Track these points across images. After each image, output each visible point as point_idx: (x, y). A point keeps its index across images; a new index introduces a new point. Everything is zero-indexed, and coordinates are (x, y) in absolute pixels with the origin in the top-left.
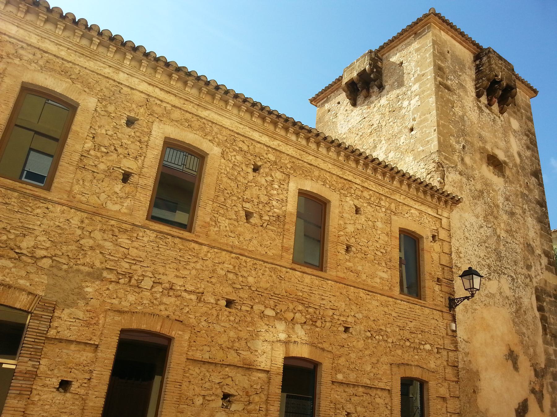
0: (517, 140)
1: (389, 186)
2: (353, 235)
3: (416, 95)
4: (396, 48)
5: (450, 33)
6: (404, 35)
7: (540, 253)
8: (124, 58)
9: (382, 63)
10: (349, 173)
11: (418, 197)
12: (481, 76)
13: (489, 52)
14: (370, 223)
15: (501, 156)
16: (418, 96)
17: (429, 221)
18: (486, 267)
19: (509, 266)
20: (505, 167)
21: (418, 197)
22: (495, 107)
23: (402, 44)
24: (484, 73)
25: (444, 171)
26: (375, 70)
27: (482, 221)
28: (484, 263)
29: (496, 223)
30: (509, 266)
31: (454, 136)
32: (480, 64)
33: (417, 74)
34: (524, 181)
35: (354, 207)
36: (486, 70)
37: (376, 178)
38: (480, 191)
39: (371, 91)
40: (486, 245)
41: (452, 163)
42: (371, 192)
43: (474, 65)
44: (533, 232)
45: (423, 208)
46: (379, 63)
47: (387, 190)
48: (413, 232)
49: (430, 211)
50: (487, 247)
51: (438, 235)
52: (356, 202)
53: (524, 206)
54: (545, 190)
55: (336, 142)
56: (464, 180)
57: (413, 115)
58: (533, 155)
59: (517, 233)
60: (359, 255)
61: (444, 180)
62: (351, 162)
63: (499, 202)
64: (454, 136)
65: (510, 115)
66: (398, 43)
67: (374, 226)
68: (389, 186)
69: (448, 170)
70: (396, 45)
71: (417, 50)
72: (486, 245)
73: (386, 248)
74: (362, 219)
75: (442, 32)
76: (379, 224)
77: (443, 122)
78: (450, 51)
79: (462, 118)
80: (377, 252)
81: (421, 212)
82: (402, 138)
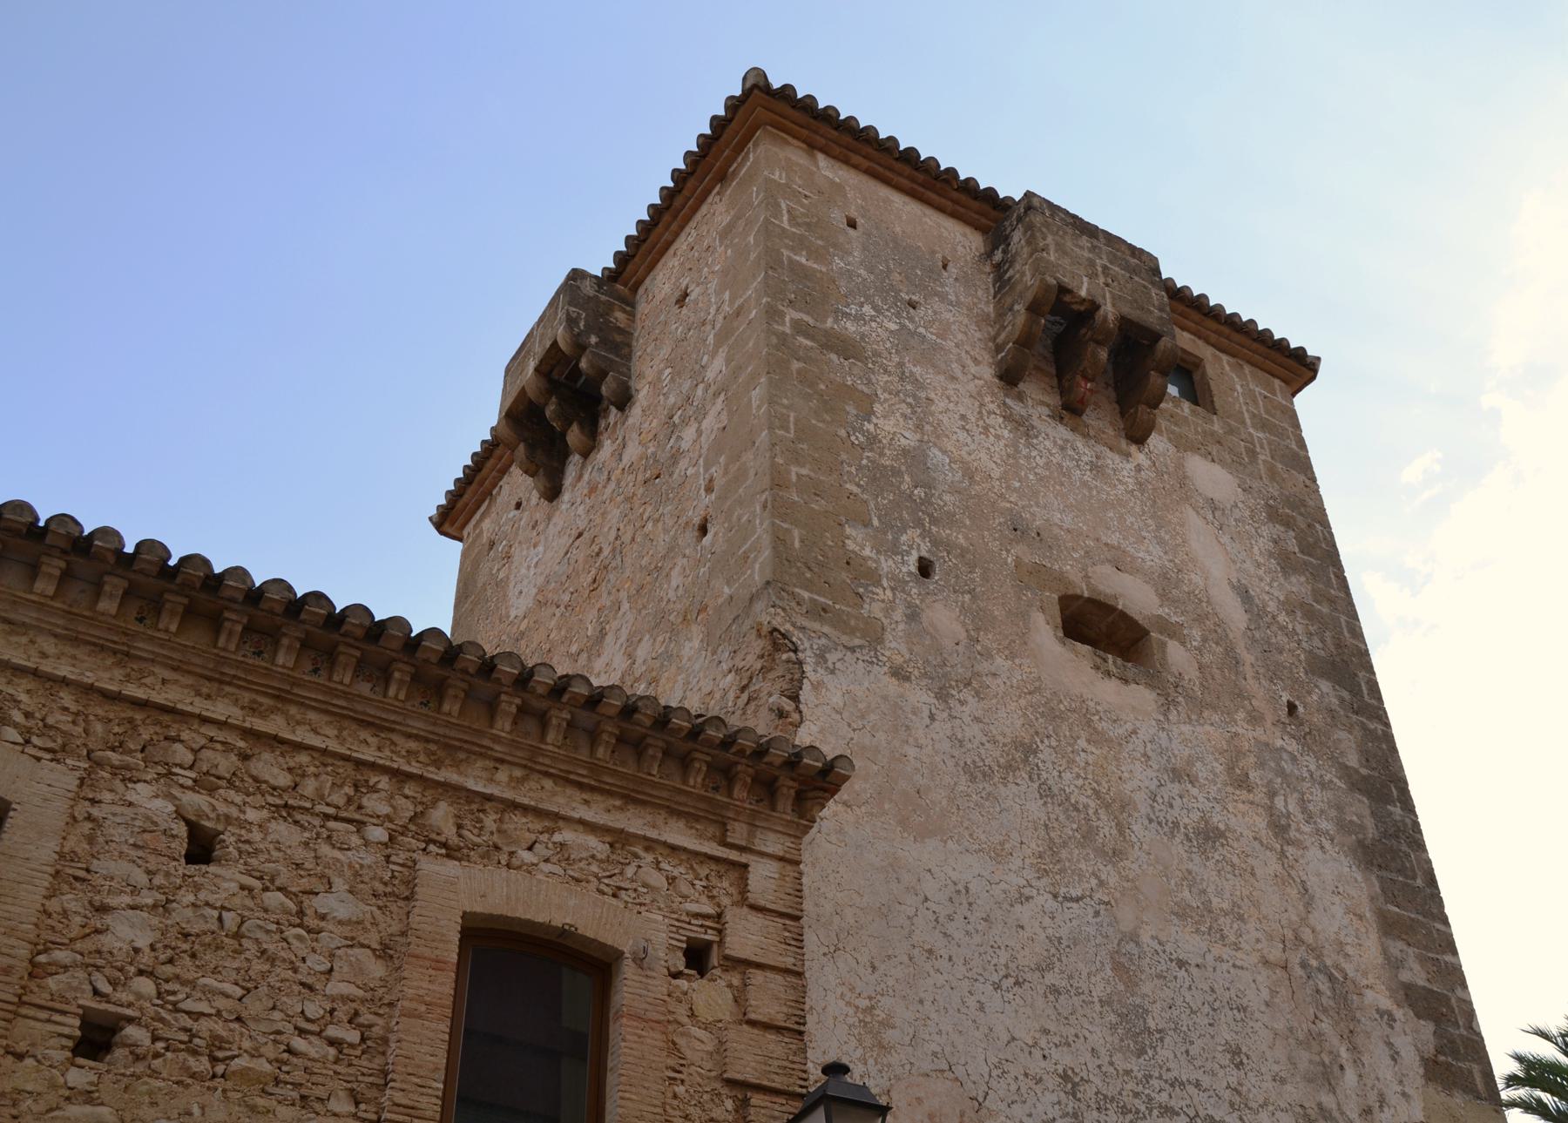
0: (1225, 539)
1: (417, 725)
2: (146, 959)
3: (716, 395)
4: (671, 251)
5: (856, 159)
6: (685, 192)
7: (1386, 1003)
8: (98, 594)
9: (632, 315)
10: (167, 674)
11: (595, 768)
12: (1009, 300)
13: (1029, 208)
14: (274, 898)
15: (1137, 597)
16: (722, 397)
17: (671, 880)
18: (1051, 1082)
19: (1199, 1075)
20: (1163, 645)
21: (595, 768)
22: (1101, 418)
23: (687, 230)
24: (1019, 288)
25: (800, 663)
26: (593, 339)
27: (1030, 874)
28: (1037, 1066)
29: (1113, 880)
30: (1199, 1075)
31: (867, 524)
32: (1003, 261)
33: (721, 317)
34: (1274, 699)
35: (181, 830)
36: (1023, 274)
37: (330, 691)
38: (1018, 744)
39: (603, 424)
40: (1050, 978)
41: (852, 632)
42: (303, 758)
43: (988, 269)
44: (1338, 910)
45: (634, 822)
46: (619, 315)
47: (413, 745)
48: (563, 932)
49: (677, 834)
50: (1055, 990)
51: (721, 943)
52: (196, 801)
53: (1279, 802)
54: (1395, 731)
55: (579, 689)
56: (919, 696)
57: (706, 470)
58: (1319, 596)
59: (1241, 918)
60: (168, 1064)
61: (795, 698)
62: (344, 676)
63: (1128, 787)
64: (867, 524)
65: (1182, 444)
66: (674, 227)
67: (301, 913)
68: (417, 725)
69: (821, 657)
70: (667, 236)
71: (726, 233)
72: (1050, 978)
73: (366, 1018)
74: (225, 879)
75: (820, 157)
76: (338, 904)
77: (804, 471)
78: (860, 221)
79: (915, 458)
80: (299, 1043)
81: (619, 839)
82: (674, 573)
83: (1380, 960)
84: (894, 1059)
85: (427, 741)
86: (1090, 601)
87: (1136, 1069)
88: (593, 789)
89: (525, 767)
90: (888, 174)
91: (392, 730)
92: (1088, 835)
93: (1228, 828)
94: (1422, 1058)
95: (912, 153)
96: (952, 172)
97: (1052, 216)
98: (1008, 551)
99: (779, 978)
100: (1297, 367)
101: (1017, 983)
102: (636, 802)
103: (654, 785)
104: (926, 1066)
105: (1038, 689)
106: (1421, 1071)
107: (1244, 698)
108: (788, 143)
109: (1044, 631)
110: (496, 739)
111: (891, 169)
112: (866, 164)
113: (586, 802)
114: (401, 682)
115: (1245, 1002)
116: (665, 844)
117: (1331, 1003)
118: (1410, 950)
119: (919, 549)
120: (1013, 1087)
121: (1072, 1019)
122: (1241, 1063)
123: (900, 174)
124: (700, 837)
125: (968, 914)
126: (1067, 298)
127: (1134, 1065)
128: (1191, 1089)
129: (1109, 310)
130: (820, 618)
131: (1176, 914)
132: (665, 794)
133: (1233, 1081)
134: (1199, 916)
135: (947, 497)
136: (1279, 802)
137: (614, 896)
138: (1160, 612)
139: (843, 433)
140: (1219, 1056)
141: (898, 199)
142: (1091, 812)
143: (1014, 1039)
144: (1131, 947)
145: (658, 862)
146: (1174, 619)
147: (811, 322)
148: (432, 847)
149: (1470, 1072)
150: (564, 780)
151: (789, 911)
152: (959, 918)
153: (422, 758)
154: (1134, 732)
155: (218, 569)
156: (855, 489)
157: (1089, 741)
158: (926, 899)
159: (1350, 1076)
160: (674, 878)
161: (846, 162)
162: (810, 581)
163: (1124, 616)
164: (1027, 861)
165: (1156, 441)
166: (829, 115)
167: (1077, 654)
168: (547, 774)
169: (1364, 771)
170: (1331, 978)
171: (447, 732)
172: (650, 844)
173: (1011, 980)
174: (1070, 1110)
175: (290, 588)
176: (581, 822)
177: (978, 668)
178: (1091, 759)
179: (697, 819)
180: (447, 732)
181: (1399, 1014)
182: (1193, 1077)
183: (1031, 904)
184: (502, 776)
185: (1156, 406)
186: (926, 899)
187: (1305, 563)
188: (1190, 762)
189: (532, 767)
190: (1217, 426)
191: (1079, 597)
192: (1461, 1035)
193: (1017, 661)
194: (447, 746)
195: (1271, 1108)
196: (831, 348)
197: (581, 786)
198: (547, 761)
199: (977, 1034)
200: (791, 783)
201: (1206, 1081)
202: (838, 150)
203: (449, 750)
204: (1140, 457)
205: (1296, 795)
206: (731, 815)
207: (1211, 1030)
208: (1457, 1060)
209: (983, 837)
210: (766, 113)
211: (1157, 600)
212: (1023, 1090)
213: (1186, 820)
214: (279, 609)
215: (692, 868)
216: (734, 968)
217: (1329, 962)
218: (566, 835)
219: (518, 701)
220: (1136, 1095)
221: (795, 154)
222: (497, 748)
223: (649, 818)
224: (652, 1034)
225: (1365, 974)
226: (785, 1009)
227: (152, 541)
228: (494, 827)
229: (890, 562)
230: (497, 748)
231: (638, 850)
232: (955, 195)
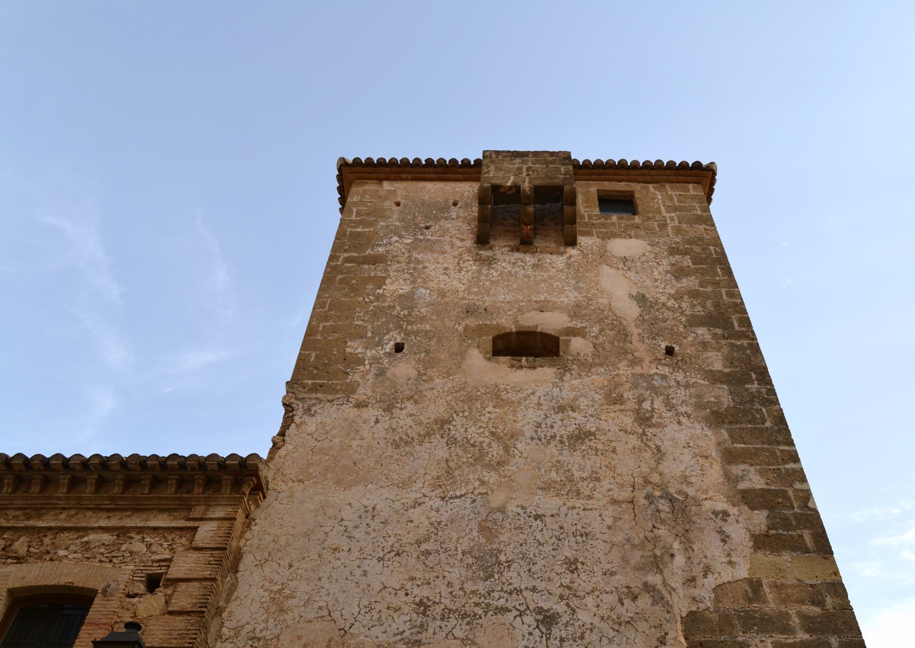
1: (19, 503)
5: (404, 176)
17: (149, 546)
41: (337, 392)
47: (18, 513)
49: (161, 521)
68: (19, 503)
81: (123, 532)
83: (721, 480)
84: (288, 617)
85: (26, 509)
86: (518, 333)
87: (481, 588)
88: (115, 510)
89: (76, 508)
90: (423, 175)
91: (8, 509)
92: (480, 459)
93: (598, 429)
94: (753, 536)
95: (429, 161)
96: (453, 161)
97: (497, 157)
98: (459, 324)
99: (197, 584)
100: (702, 176)
101: (398, 554)
102: (139, 510)
103: (148, 499)
104: (311, 616)
105: (463, 389)
106: (751, 544)
107: (628, 353)
108: (366, 183)
109: (476, 359)
110: (59, 498)
111: (424, 173)
112: (410, 176)
113: (109, 517)
114: (8, 484)
115: (589, 530)
116: (149, 528)
117: (670, 516)
118: (752, 469)
119: (395, 339)
120: (376, 616)
121: (437, 568)
122: (577, 569)
123: (429, 173)
124: (176, 519)
125: (370, 522)
126: (502, 190)
127: (481, 587)
128: (528, 594)
129: (526, 186)
130: (317, 391)
131: (542, 489)
132: (154, 502)
133: (566, 582)
134: (568, 486)
135: (423, 310)
136: (646, 405)
137: (111, 561)
138: (570, 325)
139: (361, 299)
140: (556, 567)
141: (429, 185)
142: (485, 445)
143: (385, 587)
144: (499, 516)
145: (144, 538)
146: (579, 326)
147: (356, 255)
148: (9, 561)
149: (801, 536)
150: (97, 509)
151: (218, 546)
152: (363, 527)
153: (21, 518)
154: (533, 393)
155: (30, 457)
156: (360, 323)
157: (494, 407)
158: (342, 520)
159: (680, 560)
160: (151, 545)
161: (401, 179)
162: (316, 375)
163: (544, 335)
164: (426, 483)
165: (581, 240)
166: (381, 162)
167: (498, 363)
168: (89, 509)
169: (727, 370)
170: (672, 500)
171: (34, 502)
172: (140, 530)
173: (393, 554)
174: (418, 623)
175: (6, 456)
176: (100, 528)
177: (421, 388)
178: (493, 416)
179: (175, 510)
180: (34, 502)
181: (733, 511)
182: (530, 586)
183: (423, 506)
184: (63, 516)
185: (575, 223)
186: (342, 520)
187: (696, 269)
188: (575, 399)
189: (80, 508)
190: (637, 219)
191: (510, 334)
192: (795, 514)
193: (451, 378)
194: (36, 509)
195: (597, 593)
196: (364, 263)
197: (108, 510)
198: (87, 502)
199: (357, 590)
200: (228, 477)
201: (541, 585)
202: (393, 176)
203: (38, 511)
204: (572, 251)
205: (661, 398)
206: (195, 503)
207: (554, 553)
208: (788, 530)
209: (396, 477)
210: (353, 174)
211: (568, 319)
212: (383, 618)
213: (563, 432)
214: (216, 468)
215: (164, 537)
216: (172, 585)
217: (672, 491)
218: (92, 537)
219: (69, 476)
220: (477, 605)
221: (371, 187)
222: (60, 502)
223: (145, 516)
224: (99, 631)
225: (706, 491)
226: (194, 601)
227: (133, 455)
228: (49, 542)
229: (374, 351)
230: (60, 502)
231: (133, 535)
232: (461, 170)
